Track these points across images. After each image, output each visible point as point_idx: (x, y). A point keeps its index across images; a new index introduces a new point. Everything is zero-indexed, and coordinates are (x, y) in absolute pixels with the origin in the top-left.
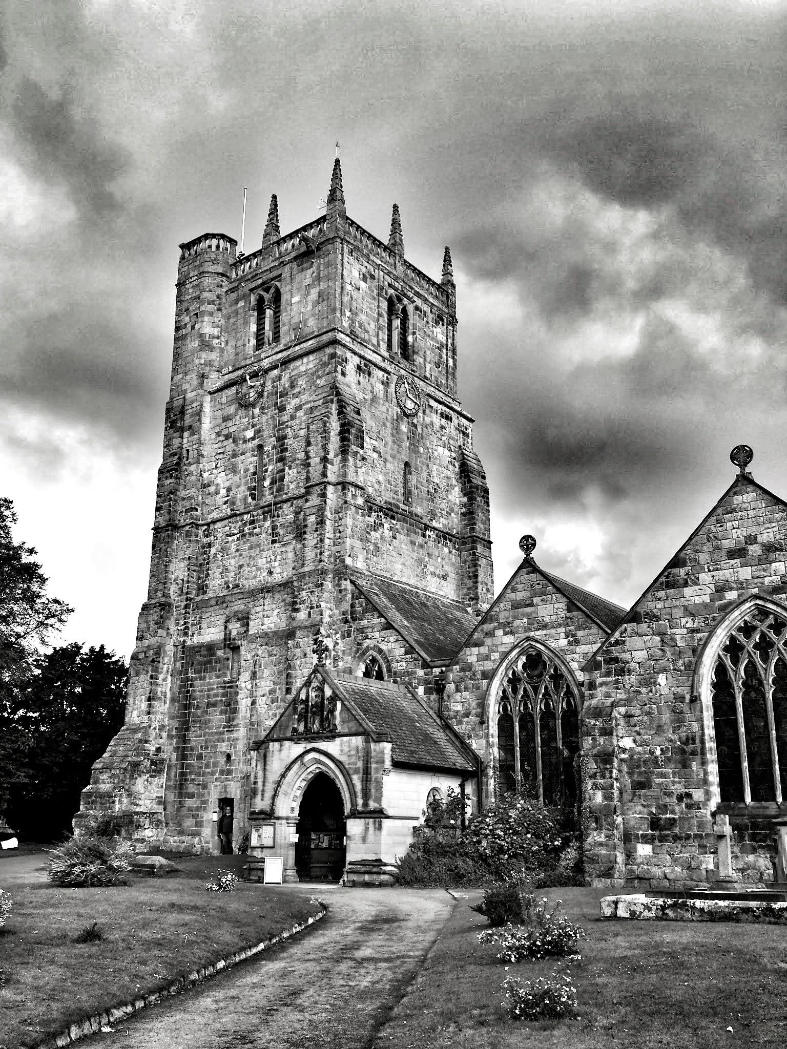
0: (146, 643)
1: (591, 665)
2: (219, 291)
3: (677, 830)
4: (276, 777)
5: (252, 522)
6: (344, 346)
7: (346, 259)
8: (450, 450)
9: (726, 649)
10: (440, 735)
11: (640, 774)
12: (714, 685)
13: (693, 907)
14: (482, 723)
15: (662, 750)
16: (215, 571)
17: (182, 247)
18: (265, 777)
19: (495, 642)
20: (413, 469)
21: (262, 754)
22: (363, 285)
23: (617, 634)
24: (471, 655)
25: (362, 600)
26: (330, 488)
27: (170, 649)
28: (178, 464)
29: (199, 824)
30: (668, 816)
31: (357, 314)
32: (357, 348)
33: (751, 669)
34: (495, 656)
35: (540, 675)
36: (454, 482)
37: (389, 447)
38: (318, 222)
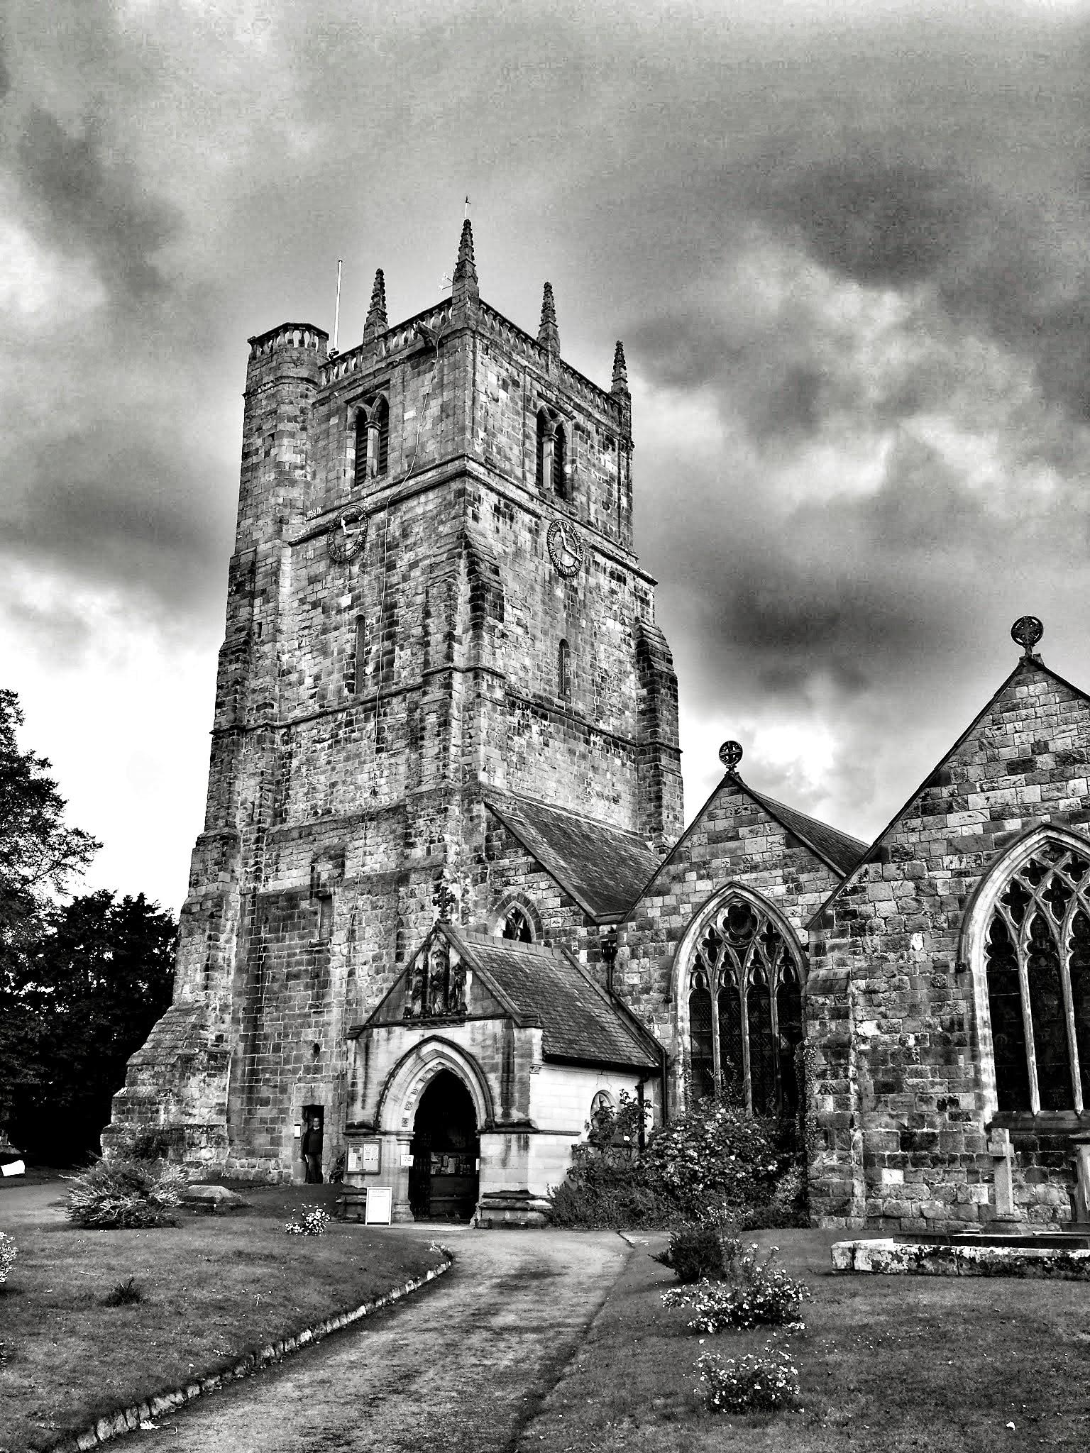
0: (202, 890)
1: (819, 921)
2: (303, 403)
3: (937, 1150)
4: (383, 1077)
5: (349, 723)
6: (477, 479)
7: (479, 359)
8: (623, 624)
9: (1006, 899)
10: (609, 1019)
11: (886, 1071)
12: (989, 949)
13: (960, 1257)
14: (667, 1001)
15: (916, 1038)
16: (298, 792)
17: (253, 342)
18: (366, 1076)
19: (686, 890)
20: (572, 650)
21: (363, 1045)
22: (502, 395)
23: (855, 879)
24: (653, 907)
25: (502, 831)
26: (457, 677)
27: (235, 899)
28: (246, 643)
29: (276, 1142)
30: (925, 1130)
31: (494, 435)
32: (495, 482)
33: (1041, 927)
34: (686, 909)
35: (749, 935)
36: (629, 668)
37: (539, 619)
38: (441, 307)
